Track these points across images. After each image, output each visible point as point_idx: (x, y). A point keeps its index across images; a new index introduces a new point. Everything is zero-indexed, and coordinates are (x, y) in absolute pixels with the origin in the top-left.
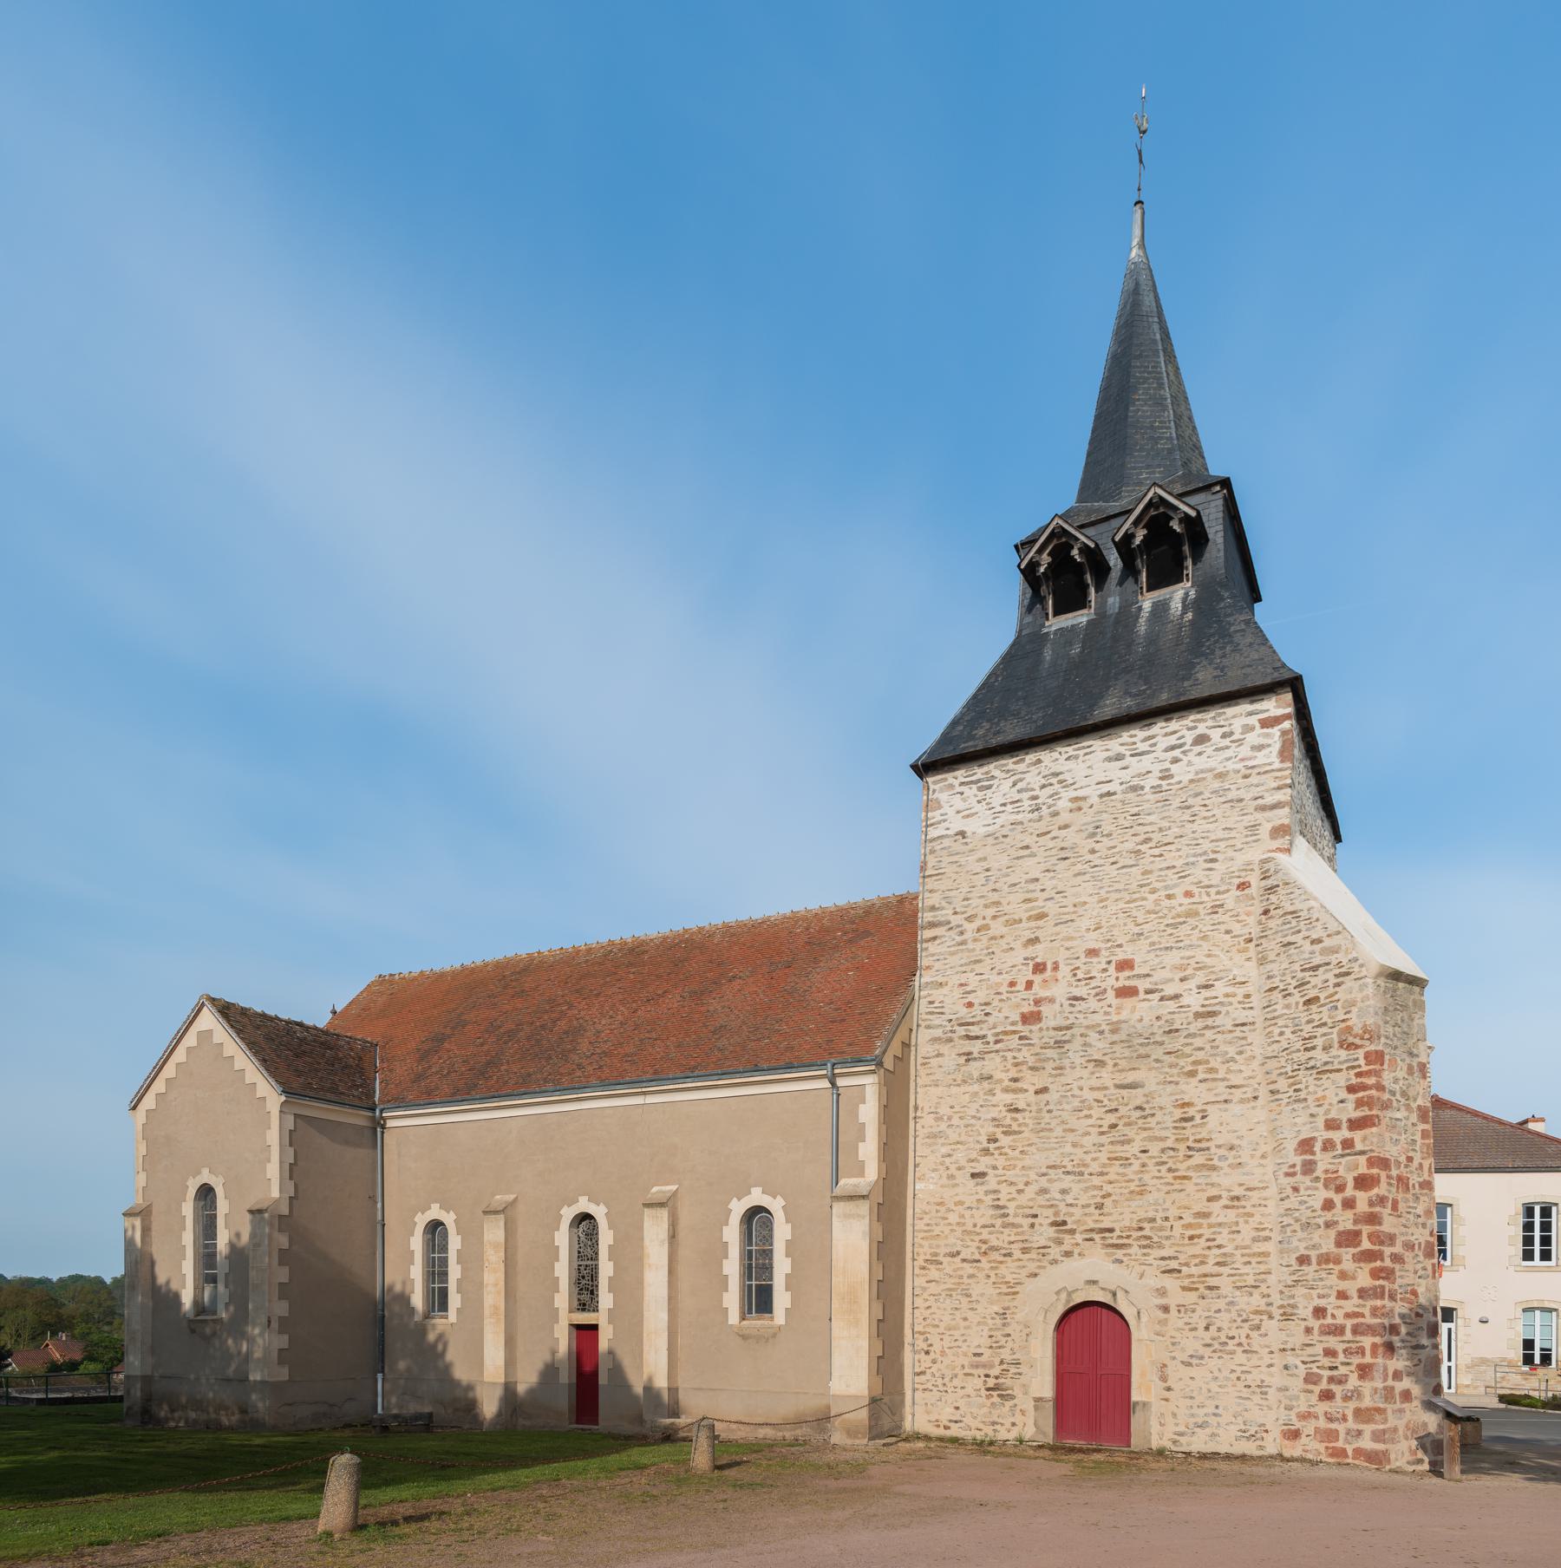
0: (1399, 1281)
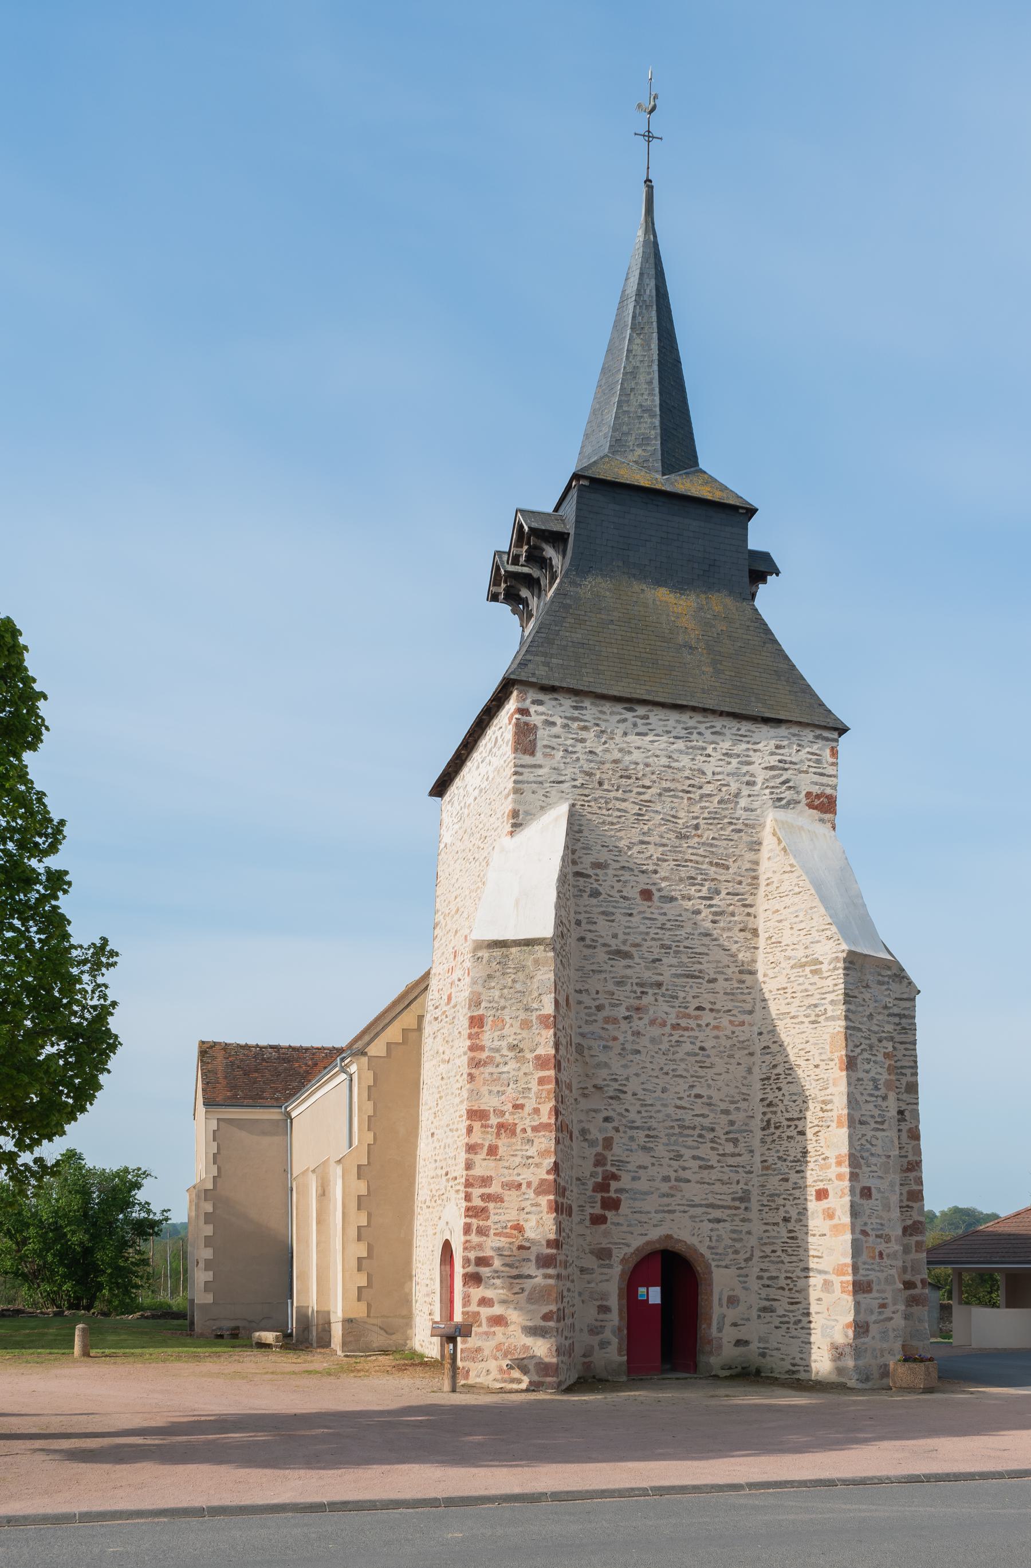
0: (493, 1218)
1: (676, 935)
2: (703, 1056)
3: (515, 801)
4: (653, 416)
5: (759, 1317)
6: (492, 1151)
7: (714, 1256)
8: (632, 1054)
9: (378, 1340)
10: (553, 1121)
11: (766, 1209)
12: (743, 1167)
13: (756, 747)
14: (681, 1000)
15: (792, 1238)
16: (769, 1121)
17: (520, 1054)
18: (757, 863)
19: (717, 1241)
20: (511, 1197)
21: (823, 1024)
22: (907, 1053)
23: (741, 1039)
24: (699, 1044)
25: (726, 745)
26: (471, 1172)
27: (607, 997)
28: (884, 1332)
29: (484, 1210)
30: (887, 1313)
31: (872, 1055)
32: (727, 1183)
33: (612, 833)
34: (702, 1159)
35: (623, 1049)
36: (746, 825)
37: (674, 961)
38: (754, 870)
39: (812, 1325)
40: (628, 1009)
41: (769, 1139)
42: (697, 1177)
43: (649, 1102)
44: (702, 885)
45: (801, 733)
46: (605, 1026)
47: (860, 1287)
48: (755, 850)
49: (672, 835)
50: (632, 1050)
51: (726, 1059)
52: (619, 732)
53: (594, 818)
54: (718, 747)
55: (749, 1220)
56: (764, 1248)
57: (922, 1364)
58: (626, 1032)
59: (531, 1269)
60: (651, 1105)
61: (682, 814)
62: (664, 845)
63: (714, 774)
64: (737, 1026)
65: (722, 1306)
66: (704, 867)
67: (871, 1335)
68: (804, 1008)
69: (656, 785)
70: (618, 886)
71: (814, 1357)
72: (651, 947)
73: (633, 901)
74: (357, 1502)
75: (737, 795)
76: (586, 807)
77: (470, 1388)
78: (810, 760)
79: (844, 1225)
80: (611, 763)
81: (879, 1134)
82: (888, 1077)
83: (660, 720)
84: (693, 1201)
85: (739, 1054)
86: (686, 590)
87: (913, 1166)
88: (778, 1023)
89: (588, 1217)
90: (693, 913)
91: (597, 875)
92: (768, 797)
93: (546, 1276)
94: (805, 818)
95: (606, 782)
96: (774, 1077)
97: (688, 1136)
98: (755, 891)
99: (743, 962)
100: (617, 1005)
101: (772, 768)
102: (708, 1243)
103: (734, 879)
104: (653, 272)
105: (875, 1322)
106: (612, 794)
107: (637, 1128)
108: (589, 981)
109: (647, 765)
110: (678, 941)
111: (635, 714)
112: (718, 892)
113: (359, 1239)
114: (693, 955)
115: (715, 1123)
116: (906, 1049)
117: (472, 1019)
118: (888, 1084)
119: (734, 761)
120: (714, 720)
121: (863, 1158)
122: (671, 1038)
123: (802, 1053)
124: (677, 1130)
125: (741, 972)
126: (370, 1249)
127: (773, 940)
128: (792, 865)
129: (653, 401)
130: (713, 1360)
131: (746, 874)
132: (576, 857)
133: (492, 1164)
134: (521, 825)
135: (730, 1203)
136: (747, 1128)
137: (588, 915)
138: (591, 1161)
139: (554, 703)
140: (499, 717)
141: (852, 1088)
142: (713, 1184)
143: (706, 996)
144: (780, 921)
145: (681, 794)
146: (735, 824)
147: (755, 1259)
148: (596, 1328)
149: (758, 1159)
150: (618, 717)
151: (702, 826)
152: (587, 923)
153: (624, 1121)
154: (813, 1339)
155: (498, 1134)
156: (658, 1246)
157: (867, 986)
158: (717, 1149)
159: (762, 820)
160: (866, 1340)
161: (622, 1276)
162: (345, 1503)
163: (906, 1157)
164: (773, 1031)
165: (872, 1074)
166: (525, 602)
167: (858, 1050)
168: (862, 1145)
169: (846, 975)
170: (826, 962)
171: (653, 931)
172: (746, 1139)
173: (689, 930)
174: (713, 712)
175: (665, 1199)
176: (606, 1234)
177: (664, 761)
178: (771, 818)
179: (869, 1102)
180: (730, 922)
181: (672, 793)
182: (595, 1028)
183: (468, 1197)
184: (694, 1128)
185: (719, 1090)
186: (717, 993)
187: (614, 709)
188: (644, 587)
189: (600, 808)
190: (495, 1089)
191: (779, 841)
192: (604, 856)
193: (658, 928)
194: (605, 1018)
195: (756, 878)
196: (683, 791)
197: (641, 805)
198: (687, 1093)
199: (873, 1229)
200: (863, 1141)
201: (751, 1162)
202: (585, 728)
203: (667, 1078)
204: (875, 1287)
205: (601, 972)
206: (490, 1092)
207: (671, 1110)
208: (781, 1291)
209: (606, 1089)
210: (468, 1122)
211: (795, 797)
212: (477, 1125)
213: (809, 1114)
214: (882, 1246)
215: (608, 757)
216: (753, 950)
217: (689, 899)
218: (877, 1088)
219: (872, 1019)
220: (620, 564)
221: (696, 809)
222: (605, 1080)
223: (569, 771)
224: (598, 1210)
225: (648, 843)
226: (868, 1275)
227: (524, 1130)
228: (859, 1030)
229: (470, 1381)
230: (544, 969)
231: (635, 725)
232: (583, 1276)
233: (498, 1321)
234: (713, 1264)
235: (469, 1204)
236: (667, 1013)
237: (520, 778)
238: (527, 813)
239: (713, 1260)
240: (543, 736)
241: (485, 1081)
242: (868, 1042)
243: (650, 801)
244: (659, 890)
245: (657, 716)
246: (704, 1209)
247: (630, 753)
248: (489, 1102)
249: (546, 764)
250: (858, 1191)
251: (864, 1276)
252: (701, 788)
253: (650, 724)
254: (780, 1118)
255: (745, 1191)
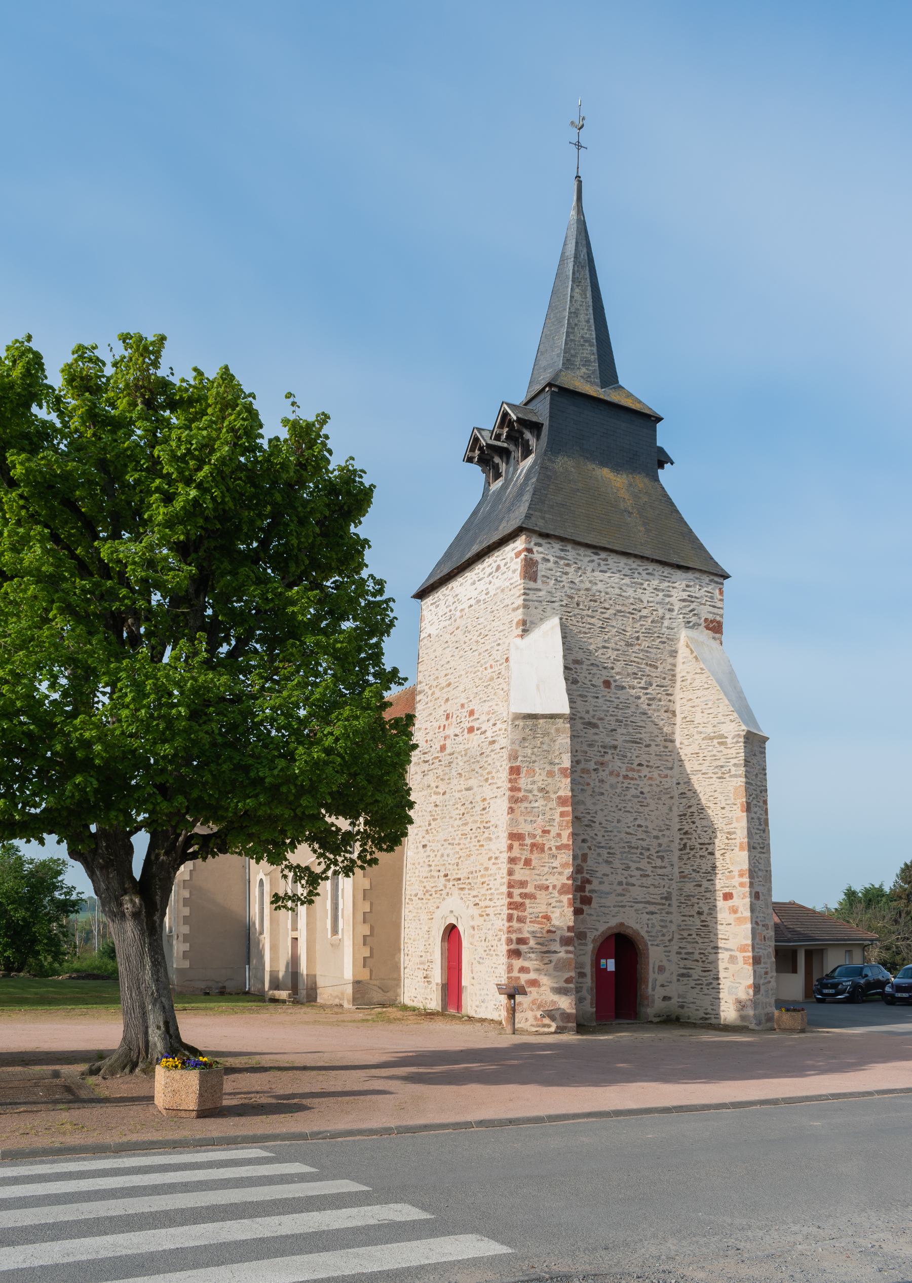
0: (529, 910)
3: (524, 614)
4: (591, 345)
5: (678, 980)
6: (528, 862)
9: (377, 996)
10: (571, 843)
11: (684, 905)
13: (674, 585)
15: (704, 926)
16: (685, 845)
18: (675, 665)
20: (541, 895)
21: (728, 779)
24: (640, 790)
29: (522, 904)
35: (593, 792)
37: (624, 731)
39: (721, 986)
40: (595, 764)
41: (685, 857)
44: (641, 679)
49: (623, 643)
52: (589, 569)
53: (574, 628)
55: (670, 913)
56: (682, 933)
59: (556, 946)
62: (618, 650)
71: (722, 1008)
74: (687, 1106)
75: (662, 618)
77: (523, 1032)
79: (745, 918)
85: (665, 798)
88: (692, 777)
93: (567, 952)
94: (704, 635)
96: (689, 814)
101: (684, 600)
102: (646, 929)
104: (584, 242)
105: (763, 984)
106: (585, 613)
107: (602, 847)
113: (364, 922)
117: (511, 768)
119: (661, 594)
123: (711, 798)
124: (627, 850)
125: (665, 740)
126: (372, 929)
127: (688, 719)
128: (702, 669)
129: (591, 334)
133: (528, 872)
134: (528, 631)
139: (548, 546)
140: (501, 552)
144: (693, 707)
147: (675, 940)
149: (676, 870)
150: (589, 559)
151: (641, 638)
154: (721, 996)
155: (532, 851)
157: (755, 755)
161: (592, 952)
162: (681, 1107)
164: (688, 782)
165: (758, 815)
166: (496, 468)
169: (745, 747)
170: (730, 737)
171: (611, 709)
173: (633, 710)
174: (647, 559)
177: (617, 591)
178: (684, 635)
183: (510, 895)
184: (637, 848)
188: (594, 466)
190: (529, 819)
195: (674, 676)
196: (629, 613)
202: (568, 565)
206: (525, 821)
207: (623, 835)
208: (696, 963)
210: (509, 842)
212: (516, 844)
213: (717, 841)
215: (583, 586)
218: (760, 825)
220: (578, 449)
221: (637, 625)
225: (608, 648)
227: (550, 849)
231: (599, 565)
234: (649, 943)
237: (527, 597)
238: (532, 623)
241: (522, 813)
244: (615, 681)
245: (613, 559)
246: (643, 905)
247: (596, 584)
248: (525, 828)
249: (544, 589)
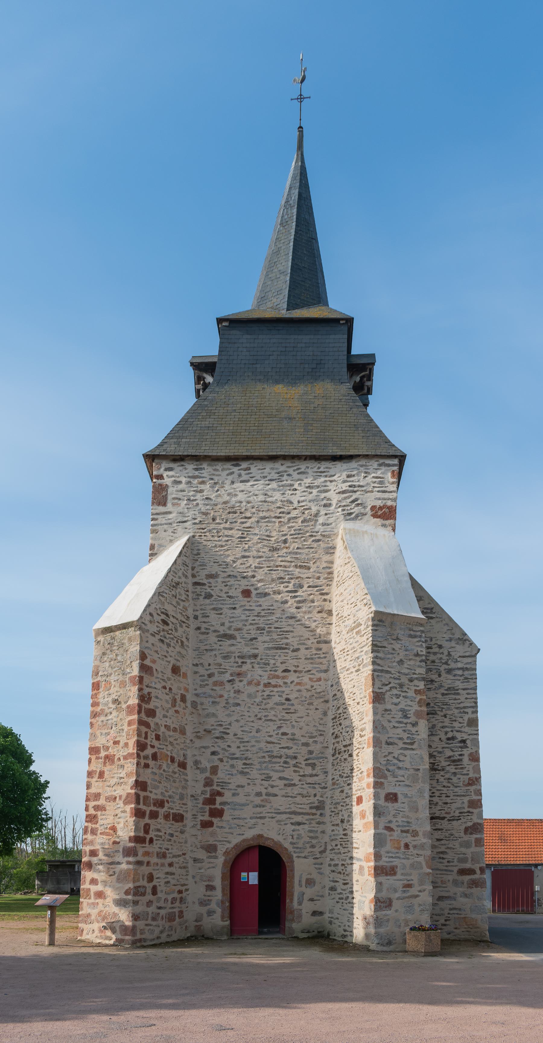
0: (100, 822)
1: (269, 620)
2: (289, 705)
7: (295, 850)
8: (234, 706)
12: (319, 784)
14: (271, 666)
17: (119, 706)
19: (298, 838)
20: (110, 806)
22: (469, 696)
23: (318, 691)
24: (285, 696)
25: (308, 481)
26: (90, 791)
27: (216, 667)
28: (409, 907)
29: (95, 816)
30: (413, 891)
31: (402, 691)
32: (306, 797)
33: (222, 553)
34: (287, 779)
36: (324, 536)
37: (267, 639)
38: (330, 568)
40: (231, 675)
42: (283, 792)
43: (246, 740)
44: (289, 582)
45: (368, 464)
46: (214, 688)
47: (382, 871)
48: (331, 553)
49: (266, 549)
50: (233, 703)
51: (307, 706)
52: (228, 482)
53: (209, 543)
54: (302, 482)
55: (323, 823)
57: (424, 933)
58: (230, 691)
59: (119, 858)
60: (248, 742)
61: (274, 534)
62: (260, 557)
63: (299, 502)
64: (315, 681)
65: (301, 886)
66: (291, 569)
67: (393, 909)
68: (353, 661)
69: (255, 515)
70: (225, 589)
72: (250, 630)
73: (236, 599)
75: (317, 515)
76: (203, 537)
78: (375, 482)
80: (222, 504)
81: (407, 752)
82: (419, 709)
83: (259, 469)
84: (279, 809)
86: (297, 383)
87: (474, 782)
89: (199, 823)
90: (282, 603)
91: (210, 583)
92: (340, 513)
93: (129, 863)
95: (218, 518)
97: (276, 763)
98: (330, 583)
99: (320, 635)
100: (223, 673)
101: (344, 492)
102: (291, 840)
103: (314, 576)
105: (398, 899)
107: (237, 758)
108: (203, 657)
109: (248, 502)
110: (270, 624)
111: (240, 468)
112: (301, 586)
114: (282, 633)
115: (297, 753)
116: (468, 694)
118: (418, 714)
119: (315, 491)
120: (300, 464)
121: (389, 771)
122: (263, 693)
124: (267, 759)
125: (318, 642)
130: (294, 925)
131: (323, 571)
132: (195, 572)
133: (101, 784)
134: (156, 554)
135: (308, 811)
136: (323, 755)
137: (203, 612)
138: (202, 782)
139: (181, 468)
141: (379, 717)
142: (296, 797)
143: (291, 661)
145: (274, 520)
146: (315, 536)
147: (328, 851)
148: (205, 901)
150: (228, 472)
152: (203, 617)
153: (227, 754)
156: (252, 842)
157: (398, 639)
158: (299, 772)
159: (336, 531)
160: (388, 912)
163: (468, 774)
167: (387, 688)
168: (388, 760)
172: (322, 764)
175: (258, 809)
176: (213, 834)
177: (261, 498)
179: (398, 727)
180: (310, 607)
181: (267, 520)
182: (207, 690)
185: (300, 729)
186: (300, 658)
187: (225, 467)
189: (213, 536)
190: (104, 732)
191: (344, 542)
192: (215, 569)
193: (255, 616)
194: (214, 682)
195: (331, 573)
196: (276, 517)
197: (243, 531)
198: (276, 732)
199: (398, 826)
200: (390, 758)
201: (326, 780)
202: (203, 483)
203: (260, 722)
204: (399, 871)
205: (212, 650)
209: (213, 732)
211: (362, 511)
212: (93, 757)
214: (409, 839)
215: (220, 500)
216: (328, 626)
217: (279, 593)
219: (403, 664)
220: (250, 374)
221: (285, 529)
222: (213, 725)
223: (191, 514)
224: (206, 818)
225: (249, 557)
226: (392, 862)
227: (119, 759)
228: (387, 672)
229: (83, 938)
230: (134, 644)
231: (240, 475)
232: (195, 864)
233: (100, 895)
234: (295, 855)
235: (88, 813)
236: (261, 676)
239: (295, 852)
240: (172, 492)
242: (397, 681)
243: (250, 527)
244: (256, 589)
245: (256, 468)
246: (288, 816)
247: (236, 495)
248: (101, 741)
250: (382, 796)
251: (387, 862)
252: (289, 513)
253: (251, 473)
254: (340, 747)
255: (320, 802)
